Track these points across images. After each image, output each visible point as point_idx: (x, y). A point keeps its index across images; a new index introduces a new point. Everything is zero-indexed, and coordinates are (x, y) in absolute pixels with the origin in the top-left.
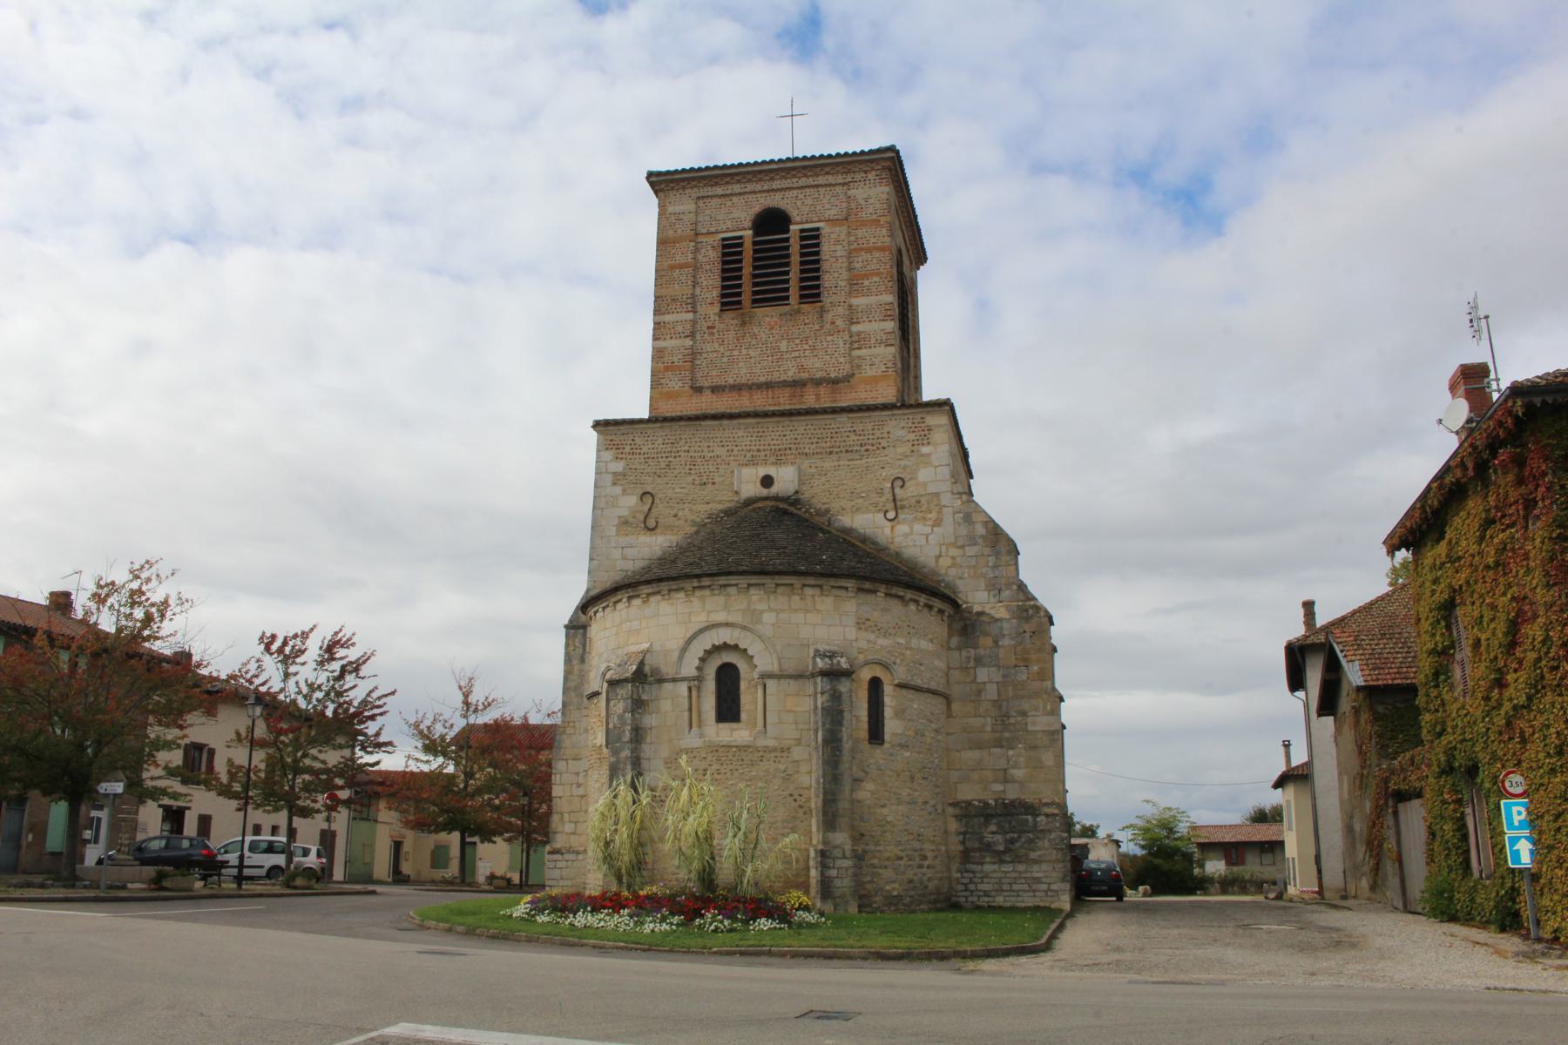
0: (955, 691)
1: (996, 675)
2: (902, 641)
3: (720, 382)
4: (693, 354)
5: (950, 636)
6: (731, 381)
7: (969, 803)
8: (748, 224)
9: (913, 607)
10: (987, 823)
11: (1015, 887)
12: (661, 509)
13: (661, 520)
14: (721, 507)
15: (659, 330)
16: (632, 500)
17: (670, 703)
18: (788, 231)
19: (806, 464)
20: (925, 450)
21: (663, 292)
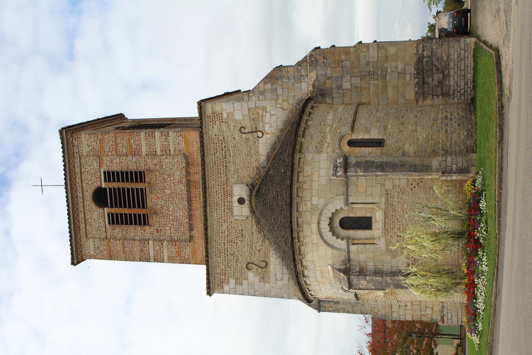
0: (355, 100)
1: (347, 78)
2: (328, 129)
3: (187, 226)
4: (172, 241)
5: (326, 103)
6: (187, 220)
7: (416, 93)
8: (101, 210)
9: (310, 123)
10: (427, 83)
11: (462, 68)
12: (255, 259)
13: (262, 259)
14: (255, 226)
15: (158, 259)
16: (251, 275)
17: (361, 255)
18: (105, 189)
19: (232, 180)
20: (225, 116)
21: (137, 257)
